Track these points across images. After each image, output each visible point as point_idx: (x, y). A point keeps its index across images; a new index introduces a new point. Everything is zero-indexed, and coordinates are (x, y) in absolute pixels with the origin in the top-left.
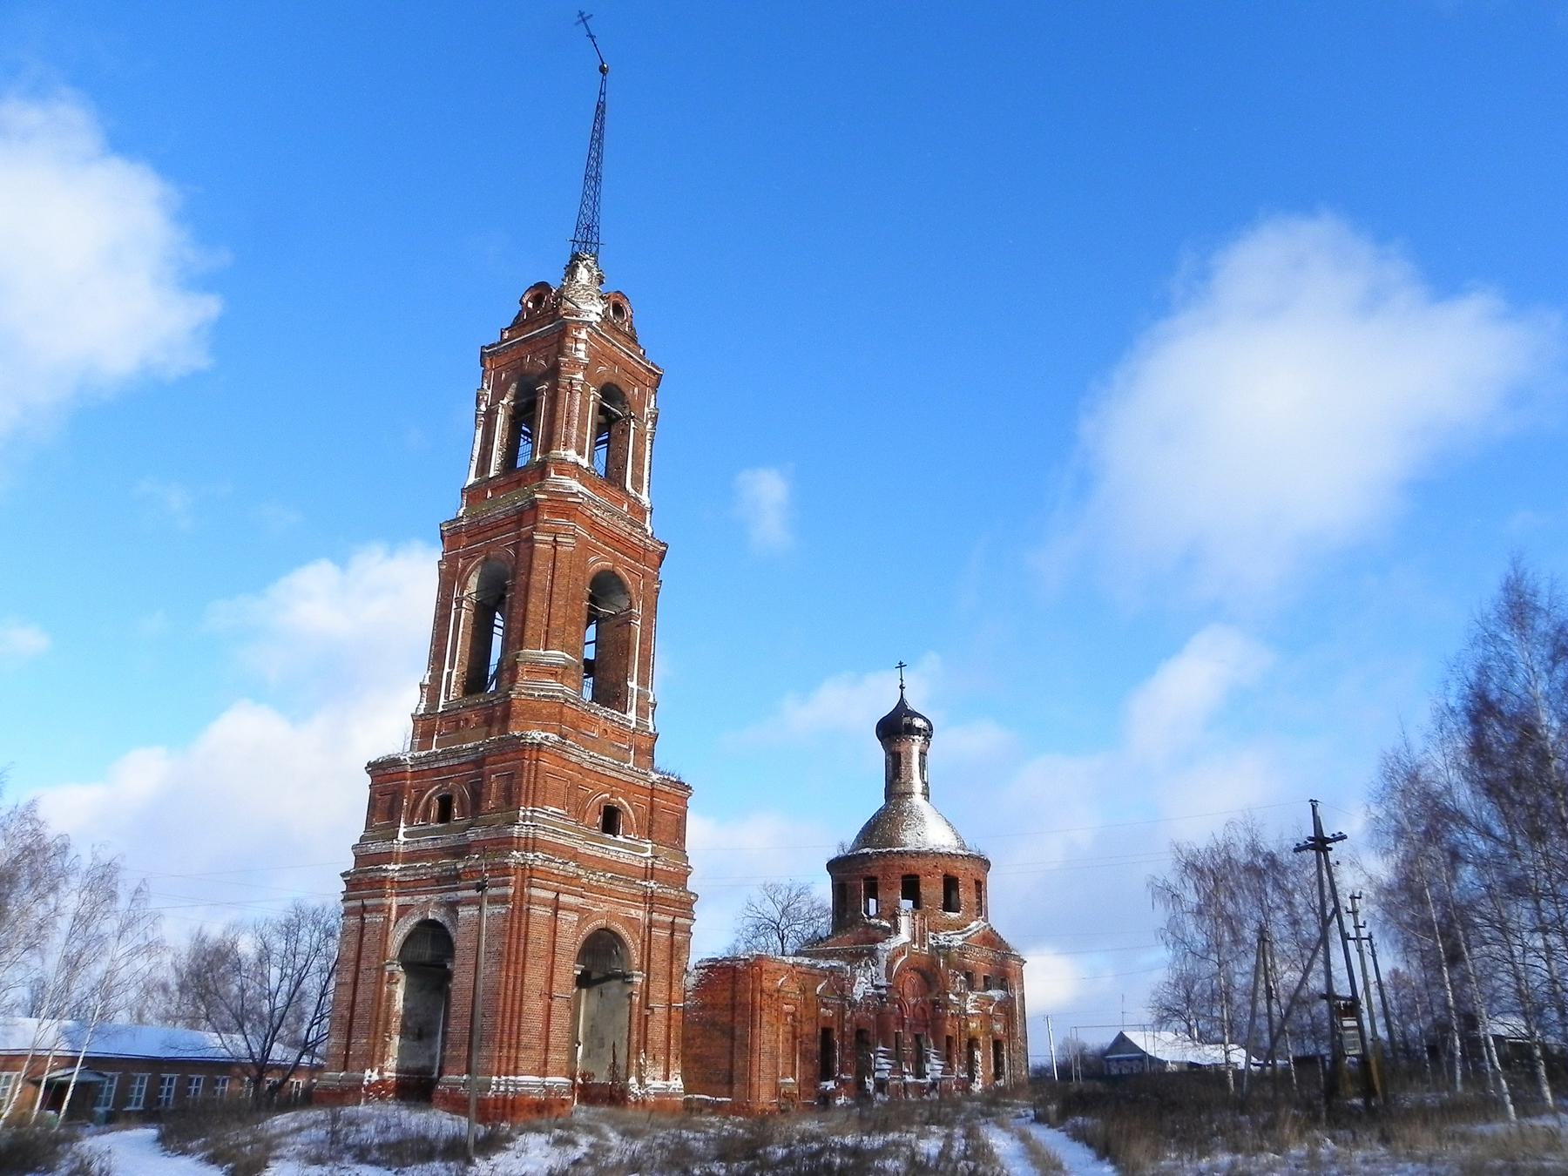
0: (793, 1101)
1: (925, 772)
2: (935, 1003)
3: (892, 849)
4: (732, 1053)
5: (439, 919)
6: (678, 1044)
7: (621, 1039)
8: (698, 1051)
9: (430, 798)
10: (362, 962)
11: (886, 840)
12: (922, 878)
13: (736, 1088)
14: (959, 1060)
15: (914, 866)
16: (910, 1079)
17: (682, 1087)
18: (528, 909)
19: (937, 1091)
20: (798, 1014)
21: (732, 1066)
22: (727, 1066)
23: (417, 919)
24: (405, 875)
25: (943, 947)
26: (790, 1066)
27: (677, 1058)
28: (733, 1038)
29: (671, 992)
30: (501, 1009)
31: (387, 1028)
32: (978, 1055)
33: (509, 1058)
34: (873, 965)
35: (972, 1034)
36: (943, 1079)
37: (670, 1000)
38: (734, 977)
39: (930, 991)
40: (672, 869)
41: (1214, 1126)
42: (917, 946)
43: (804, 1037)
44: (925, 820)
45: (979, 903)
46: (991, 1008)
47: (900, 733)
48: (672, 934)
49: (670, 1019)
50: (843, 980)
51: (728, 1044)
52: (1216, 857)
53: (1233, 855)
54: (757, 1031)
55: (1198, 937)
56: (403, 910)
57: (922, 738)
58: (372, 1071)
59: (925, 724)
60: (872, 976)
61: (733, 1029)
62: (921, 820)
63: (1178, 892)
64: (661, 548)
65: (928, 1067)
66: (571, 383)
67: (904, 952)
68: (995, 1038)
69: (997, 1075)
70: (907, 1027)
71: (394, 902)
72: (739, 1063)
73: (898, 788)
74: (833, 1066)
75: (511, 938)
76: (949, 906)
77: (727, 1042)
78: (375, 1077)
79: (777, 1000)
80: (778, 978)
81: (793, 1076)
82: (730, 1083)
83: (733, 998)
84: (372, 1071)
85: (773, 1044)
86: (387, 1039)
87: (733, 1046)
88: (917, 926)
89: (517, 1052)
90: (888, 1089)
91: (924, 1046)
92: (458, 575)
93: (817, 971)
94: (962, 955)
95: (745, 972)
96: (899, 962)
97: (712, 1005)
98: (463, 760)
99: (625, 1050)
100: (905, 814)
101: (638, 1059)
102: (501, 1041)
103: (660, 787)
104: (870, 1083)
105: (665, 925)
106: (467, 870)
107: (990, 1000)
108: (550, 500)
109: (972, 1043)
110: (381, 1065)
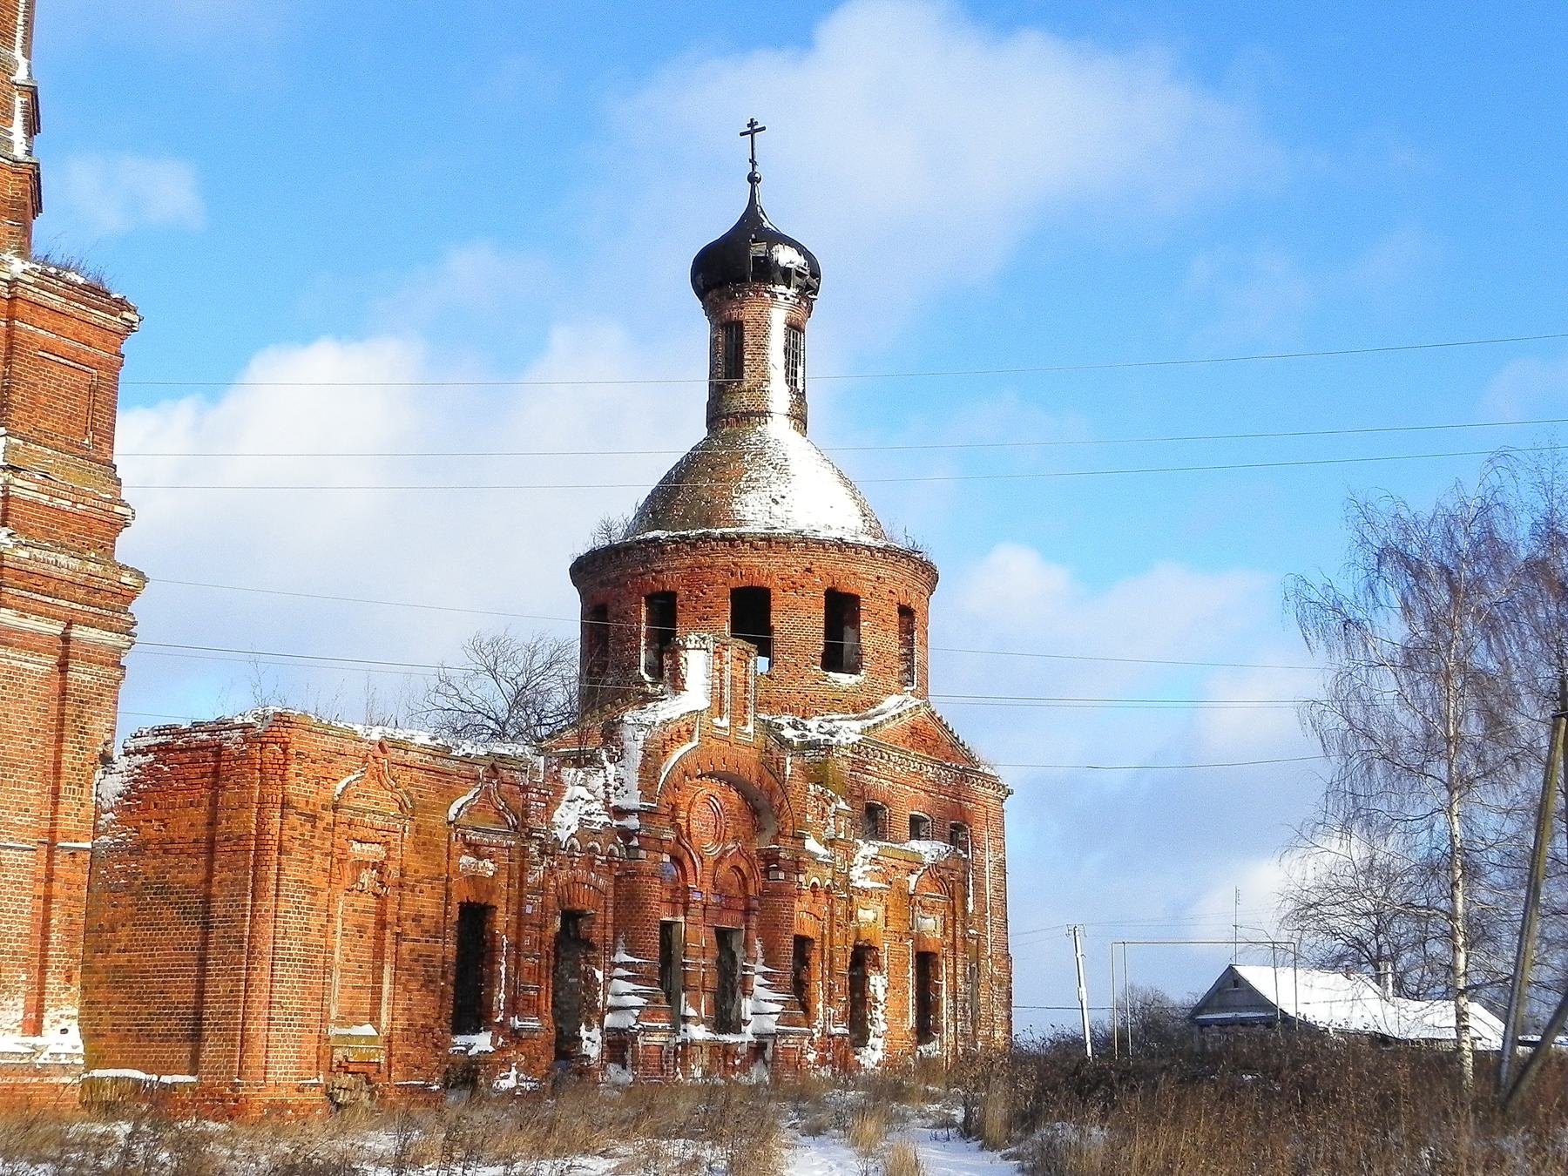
0: (369, 1082)
1: (800, 369)
2: (770, 858)
3: (713, 531)
4: (202, 961)
6: (73, 943)
8: (123, 959)
11: (701, 511)
12: (777, 594)
13: (208, 1052)
14: (830, 991)
15: (761, 568)
16: (698, 1033)
17: (81, 1050)
19: (766, 1063)
20: (393, 869)
21: (201, 993)
22: (190, 997)
25: (813, 745)
26: (366, 997)
27: (69, 979)
28: (207, 926)
29: (55, 812)
32: (877, 983)
34: (611, 760)
35: (864, 936)
36: (784, 1034)
37: (52, 833)
38: (216, 772)
39: (759, 829)
40: (66, 504)
41: (1424, 1154)
42: (725, 722)
43: (408, 924)
44: (792, 470)
45: (908, 657)
46: (913, 879)
47: (743, 279)
48: (63, 667)
49: (50, 879)
50: (525, 789)
52: (1459, 535)
53: (1502, 533)
54: (268, 904)
55: (1403, 716)
57: (792, 291)
59: (800, 260)
60: (606, 785)
61: (208, 899)
62: (781, 468)
63: (1359, 615)
65: (747, 1005)
67: (690, 732)
68: (921, 949)
69: (925, 1031)
70: (696, 911)
72: (218, 985)
73: (735, 402)
74: (491, 995)
76: (835, 659)
77: (191, 934)
79: (330, 829)
80: (335, 774)
81: (374, 1018)
82: (196, 1037)
83: (212, 823)
85: (314, 937)
87: (205, 944)
88: (727, 676)
90: (636, 1052)
91: (739, 955)
93: (451, 766)
94: (860, 765)
95: (245, 757)
96: (677, 754)
103: (34, 294)
104: (591, 1043)
105: (37, 643)
107: (914, 863)
109: (862, 957)
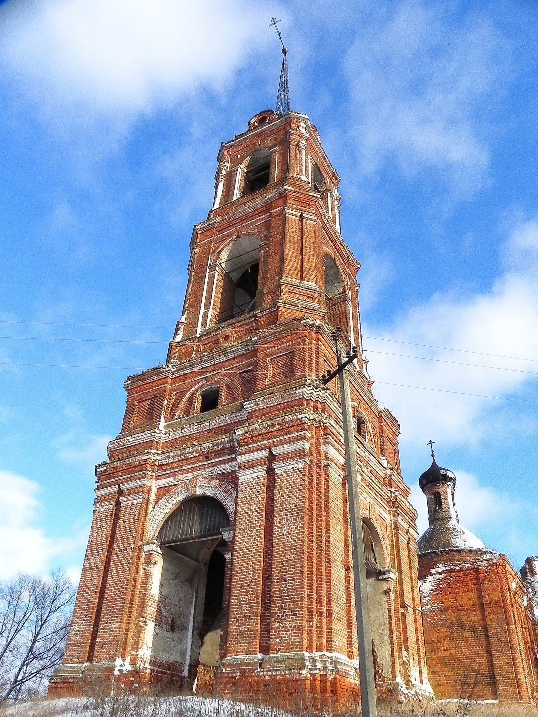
4: (489, 652)
5: (209, 493)
7: (381, 637)
8: (447, 653)
9: (193, 394)
10: (115, 544)
18: (327, 466)
21: (491, 665)
23: (181, 497)
24: (169, 457)
28: (487, 638)
30: (306, 570)
31: (141, 614)
33: (320, 630)
47: (439, 480)
51: (483, 643)
56: (163, 492)
58: (124, 660)
61: (485, 628)
62: (463, 533)
64: (357, 265)
66: (298, 145)
71: (154, 485)
75: (311, 491)
78: (127, 667)
82: (493, 682)
84: (124, 660)
86: (142, 624)
87: (488, 645)
89: (329, 622)
92: (211, 253)
97: (456, 607)
98: (231, 356)
99: (388, 648)
100: (451, 529)
101: (400, 657)
102: (310, 608)
106: (248, 435)
108: (295, 192)
110: (134, 653)
